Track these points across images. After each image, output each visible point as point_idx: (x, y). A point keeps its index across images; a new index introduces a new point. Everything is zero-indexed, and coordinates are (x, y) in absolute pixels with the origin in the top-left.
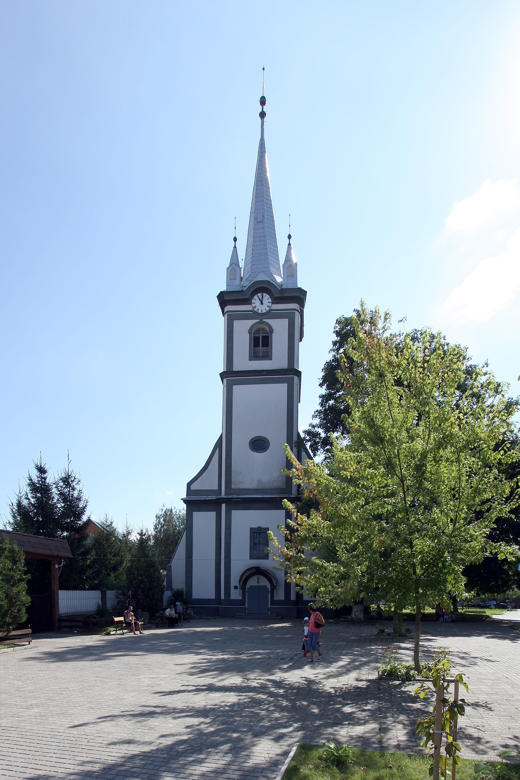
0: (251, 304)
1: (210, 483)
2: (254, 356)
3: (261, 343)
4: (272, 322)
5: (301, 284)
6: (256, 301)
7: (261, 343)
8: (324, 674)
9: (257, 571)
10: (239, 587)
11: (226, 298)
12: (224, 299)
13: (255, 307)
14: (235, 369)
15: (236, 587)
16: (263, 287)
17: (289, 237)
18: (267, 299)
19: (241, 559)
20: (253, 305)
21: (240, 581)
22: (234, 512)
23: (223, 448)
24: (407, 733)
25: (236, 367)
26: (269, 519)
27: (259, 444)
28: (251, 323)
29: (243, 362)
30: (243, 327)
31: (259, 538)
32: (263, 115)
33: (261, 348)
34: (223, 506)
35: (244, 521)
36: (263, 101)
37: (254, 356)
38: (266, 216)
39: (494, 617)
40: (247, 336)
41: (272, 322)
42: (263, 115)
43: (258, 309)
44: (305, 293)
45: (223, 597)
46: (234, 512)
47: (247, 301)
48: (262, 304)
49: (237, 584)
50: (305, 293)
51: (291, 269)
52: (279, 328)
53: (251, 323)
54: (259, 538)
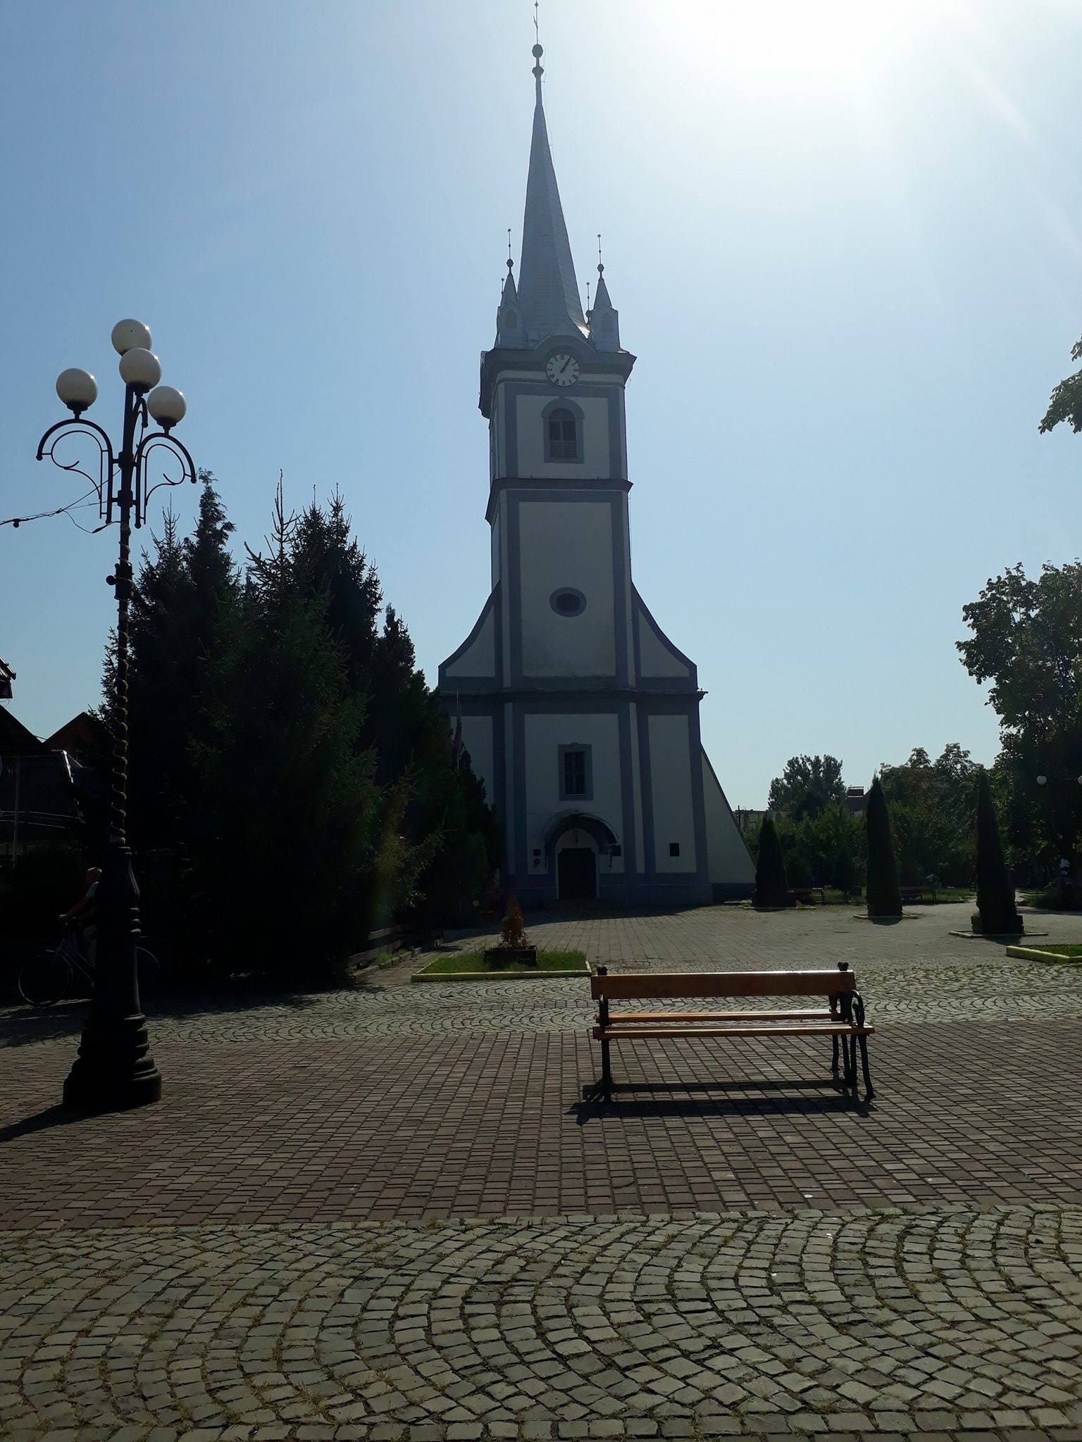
0: (545, 370)
2: (553, 454)
4: (582, 402)
6: (556, 364)
8: (989, 1342)
9: (577, 821)
14: (521, 475)
15: (537, 852)
18: (573, 367)
20: (549, 373)
22: (490, 673)
28: (544, 400)
32: (538, 71)
34: (509, 707)
36: (538, 51)
37: (553, 454)
41: (582, 402)
42: (538, 71)
46: (490, 673)
52: (591, 409)
53: (544, 400)
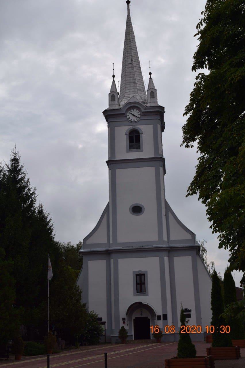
1: (101, 239)
3: (135, 139)
5: (160, 103)
7: (135, 139)
9: (138, 306)
10: (126, 319)
11: (143, 276)
12: (108, 115)
13: (129, 118)
14: (117, 158)
15: (124, 319)
16: (133, 106)
17: (150, 74)
19: (128, 296)
21: (127, 315)
23: (109, 212)
24: (46, 218)
25: (119, 157)
26: (150, 265)
27: (137, 210)
29: (124, 154)
30: (123, 132)
31: (140, 282)
33: (134, 143)
35: (127, 267)
38: (134, 60)
39: (152, 332)
40: (125, 136)
43: (131, 119)
44: (163, 108)
45: (113, 328)
47: (123, 115)
48: (134, 115)
49: (125, 316)
50: (163, 108)
51: (153, 93)
52: (146, 131)
54: (140, 282)
